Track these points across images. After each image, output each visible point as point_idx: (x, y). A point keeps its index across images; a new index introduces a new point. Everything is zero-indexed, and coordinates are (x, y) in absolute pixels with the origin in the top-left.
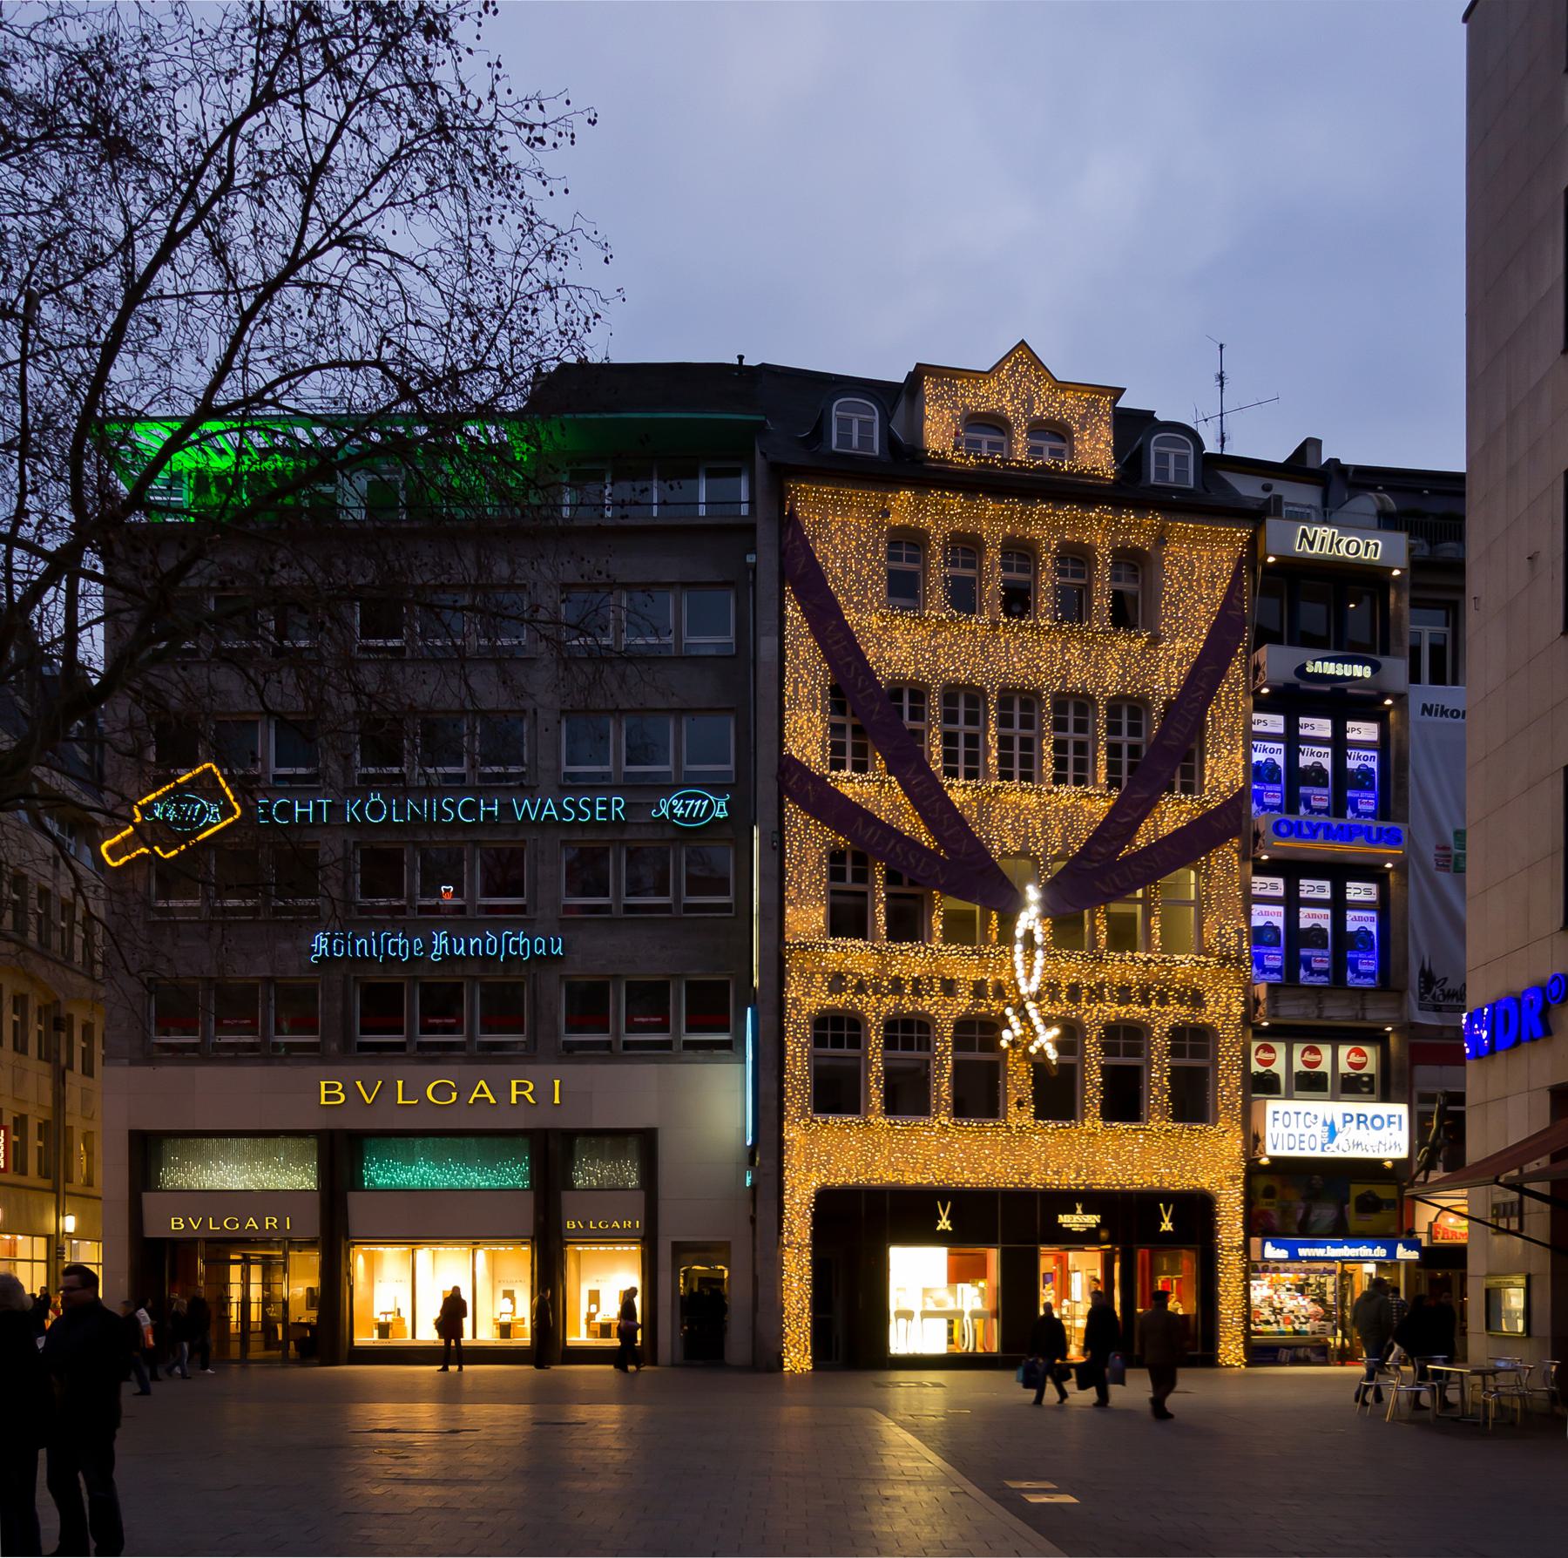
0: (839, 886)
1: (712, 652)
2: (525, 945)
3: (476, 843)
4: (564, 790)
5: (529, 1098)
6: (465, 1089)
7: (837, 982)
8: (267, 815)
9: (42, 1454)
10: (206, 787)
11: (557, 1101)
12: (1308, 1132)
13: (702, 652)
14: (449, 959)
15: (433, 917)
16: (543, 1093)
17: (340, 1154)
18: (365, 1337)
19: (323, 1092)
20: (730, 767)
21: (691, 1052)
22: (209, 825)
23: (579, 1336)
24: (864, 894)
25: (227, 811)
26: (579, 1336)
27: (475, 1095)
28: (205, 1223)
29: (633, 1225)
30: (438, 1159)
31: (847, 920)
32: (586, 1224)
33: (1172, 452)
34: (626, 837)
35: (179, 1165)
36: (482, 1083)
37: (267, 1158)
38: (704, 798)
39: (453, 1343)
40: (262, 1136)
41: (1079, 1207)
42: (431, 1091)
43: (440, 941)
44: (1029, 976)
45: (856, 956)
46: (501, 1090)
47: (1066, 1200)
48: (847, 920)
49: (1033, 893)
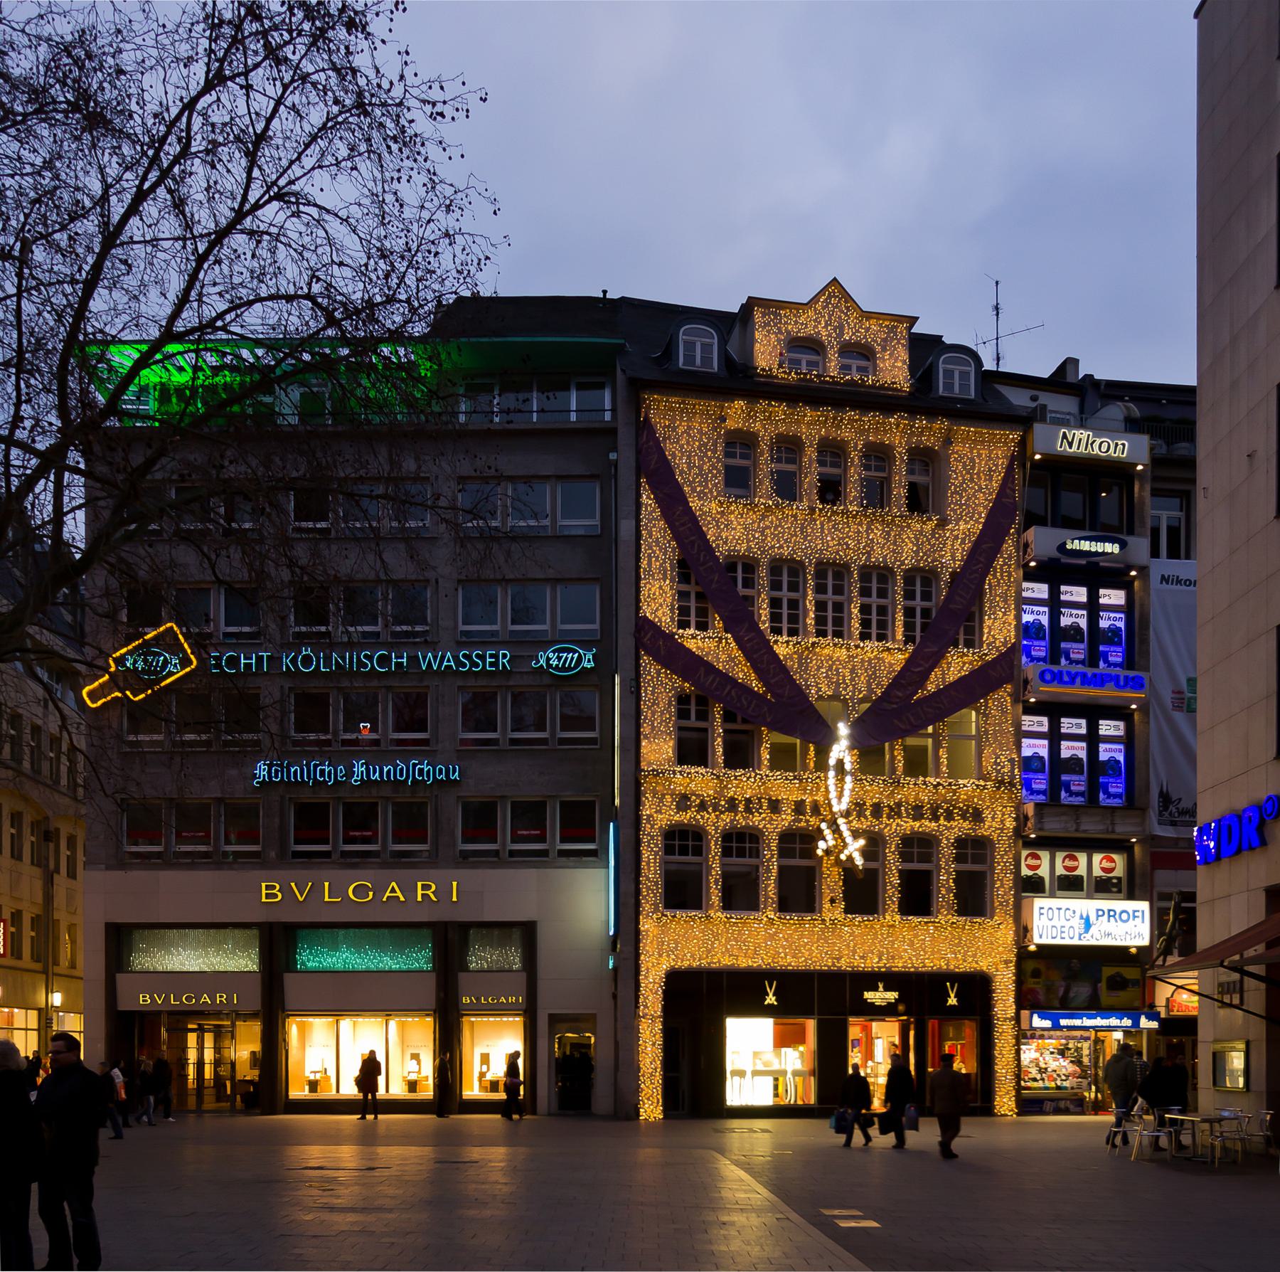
0: (685, 723)
1: (581, 532)
2: (428, 771)
3: (388, 688)
4: (461, 645)
5: (432, 896)
6: (379, 889)
7: (683, 802)
8: (218, 666)
9: (35, 1187)
10: (168, 643)
11: (455, 899)
12: (1068, 924)
13: (573, 532)
14: (367, 783)
15: (353, 749)
16: (443, 892)
17: (278, 942)
18: (298, 1092)
19: (264, 892)
20: (596, 626)
21: (564, 859)
22: (171, 674)
23: (472, 1090)
24: (705, 730)
25: (185, 662)
26: (472, 1090)
27: (388, 894)
28: (167, 999)
29: (517, 1000)
30: (357, 946)
31: (691, 751)
32: (478, 999)
33: (957, 369)
34: (511, 683)
35: (146, 951)
36: (394, 884)
37: (218, 945)
38: (574, 651)
39: (370, 1096)
40: (214, 927)
41: (881, 986)
42: (352, 891)
43: (359, 768)
44: (840, 797)
45: (699, 781)
46: (409, 890)
47: (871, 979)
48: (691, 751)
49: (843, 729)
